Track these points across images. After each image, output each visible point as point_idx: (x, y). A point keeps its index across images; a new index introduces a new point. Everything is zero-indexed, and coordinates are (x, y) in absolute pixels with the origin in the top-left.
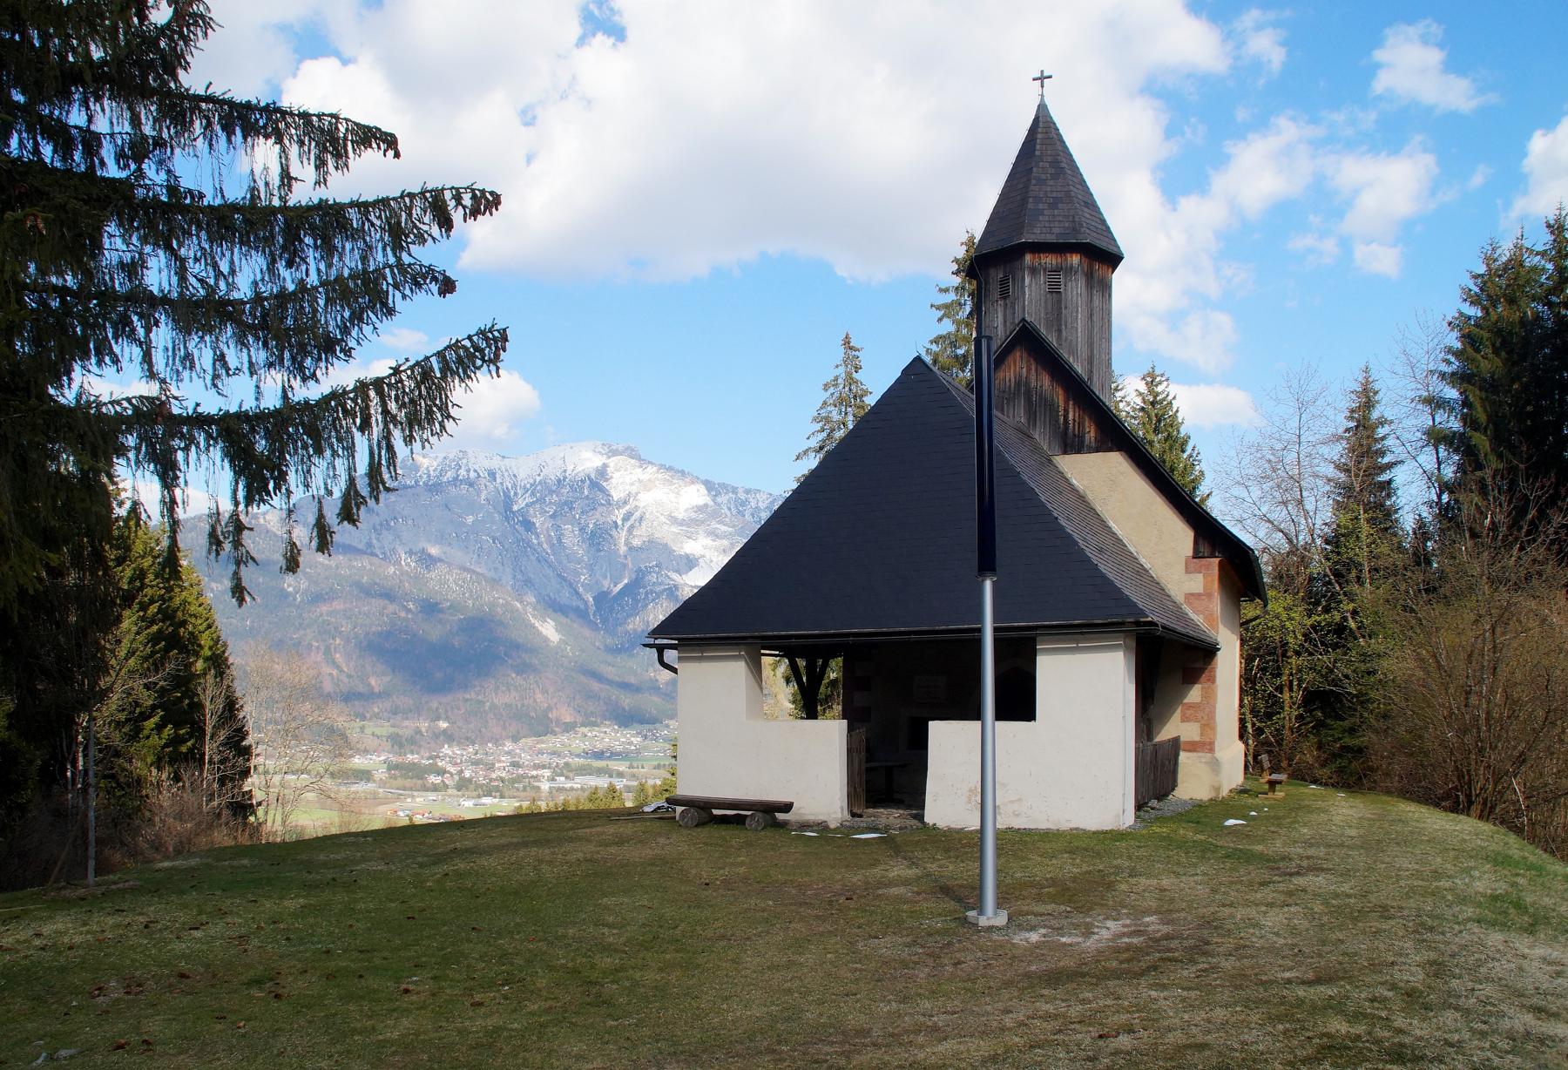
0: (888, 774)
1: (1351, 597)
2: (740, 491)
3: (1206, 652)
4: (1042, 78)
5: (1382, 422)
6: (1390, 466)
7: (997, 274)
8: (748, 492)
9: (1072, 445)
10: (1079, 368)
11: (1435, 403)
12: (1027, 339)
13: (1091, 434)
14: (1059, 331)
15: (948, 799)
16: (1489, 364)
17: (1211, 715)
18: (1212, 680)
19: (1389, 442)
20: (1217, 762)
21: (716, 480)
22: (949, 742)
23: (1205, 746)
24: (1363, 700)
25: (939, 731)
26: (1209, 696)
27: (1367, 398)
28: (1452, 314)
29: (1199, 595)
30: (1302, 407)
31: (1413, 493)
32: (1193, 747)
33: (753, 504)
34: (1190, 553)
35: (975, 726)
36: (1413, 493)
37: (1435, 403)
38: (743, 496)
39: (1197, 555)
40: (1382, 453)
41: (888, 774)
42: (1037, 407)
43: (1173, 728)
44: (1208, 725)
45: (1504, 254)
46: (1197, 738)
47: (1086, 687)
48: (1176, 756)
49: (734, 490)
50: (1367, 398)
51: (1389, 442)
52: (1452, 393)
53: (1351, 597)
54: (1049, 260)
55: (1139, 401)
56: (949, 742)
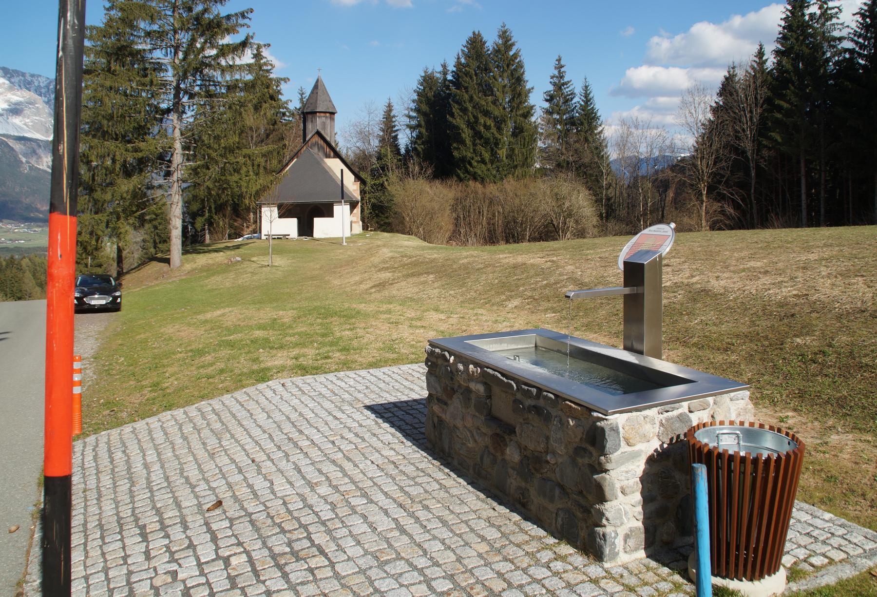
0: (306, 229)
1: (386, 175)
2: (28, 75)
5: (394, 116)
6: (397, 130)
7: (310, 116)
8: (33, 76)
9: (328, 156)
11: (410, 117)
12: (318, 133)
13: (332, 154)
15: (316, 235)
16: (425, 108)
19: (396, 123)
21: (11, 67)
22: (317, 221)
24: (389, 208)
25: (294, 221)
27: (390, 108)
28: (415, 88)
30: (370, 113)
31: (404, 139)
33: (36, 84)
36: (404, 139)
37: (410, 117)
38: (29, 79)
40: (394, 126)
41: (306, 229)
42: (320, 148)
45: (430, 72)
47: (341, 210)
49: (23, 75)
50: (390, 108)
51: (396, 123)
52: (414, 114)
53: (386, 175)
54: (322, 114)
56: (317, 221)
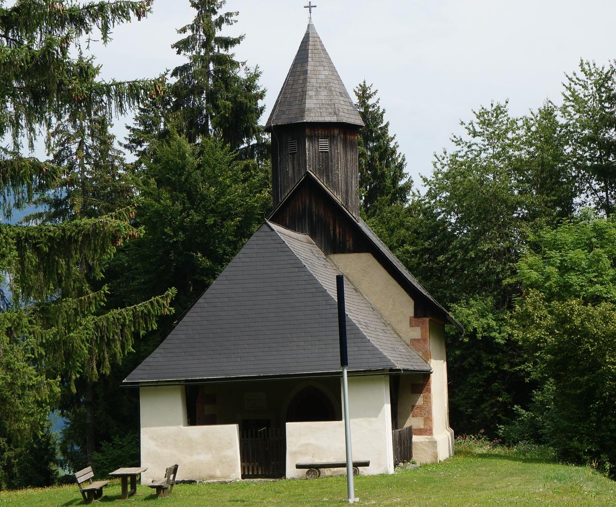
3: (425, 376)
4: (310, 7)
10: (338, 199)
13: (350, 243)
14: (328, 176)
17: (429, 412)
18: (429, 391)
20: (438, 438)
23: (428, 431)
25: (230, 433)
26: (428, 400)
29: (419, 340)
32: (421, 432)
34: (412, 315)
35: (140, 388)
39: (417, 315)
43: (413, 422)
44: (428, 419)
46: (422, 427)
48: (411, 438)
55: (128, 132)
